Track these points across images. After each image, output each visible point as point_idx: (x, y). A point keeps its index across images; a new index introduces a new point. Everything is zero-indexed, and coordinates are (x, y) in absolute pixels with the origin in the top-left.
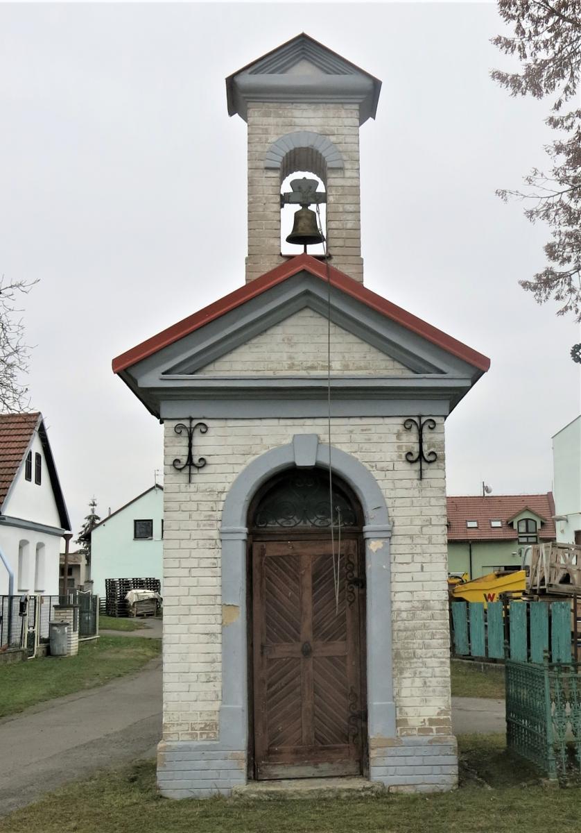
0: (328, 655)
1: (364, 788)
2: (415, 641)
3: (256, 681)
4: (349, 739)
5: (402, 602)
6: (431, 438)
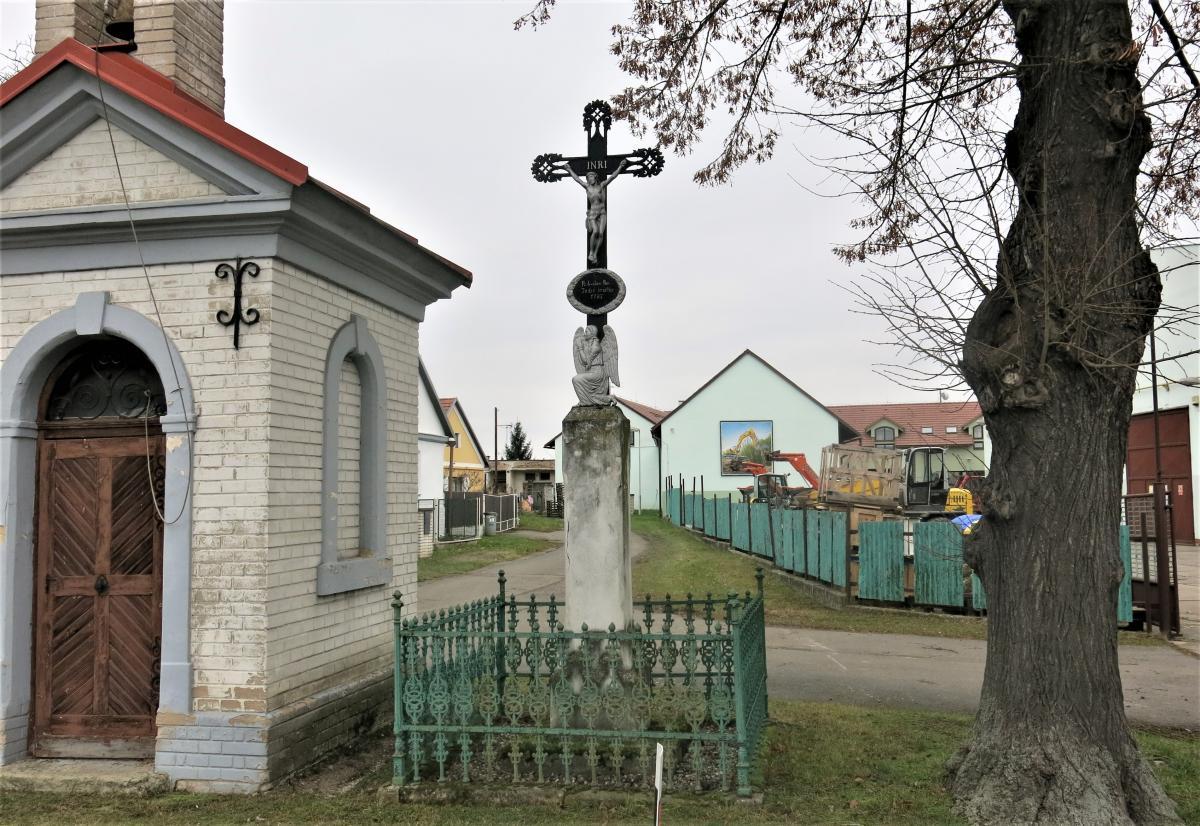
0: (128, 593)
1: (130, 782)
2: (221, 578)
3: (39, 625)
4: (133, 711)
5: (207, 522)
6: (254, 290)
